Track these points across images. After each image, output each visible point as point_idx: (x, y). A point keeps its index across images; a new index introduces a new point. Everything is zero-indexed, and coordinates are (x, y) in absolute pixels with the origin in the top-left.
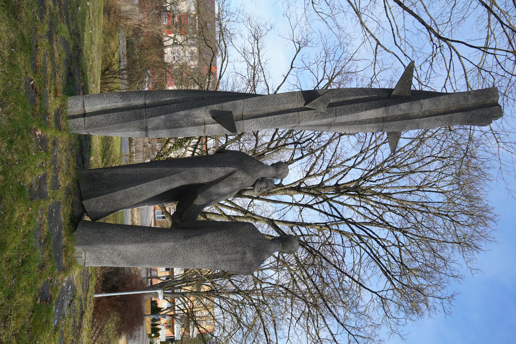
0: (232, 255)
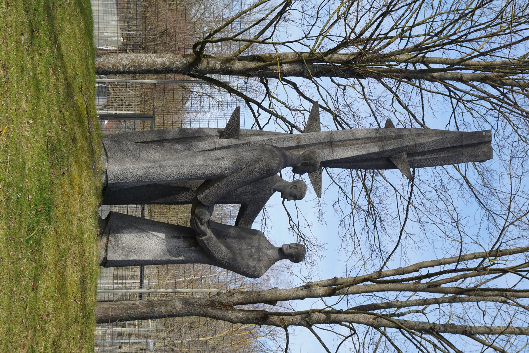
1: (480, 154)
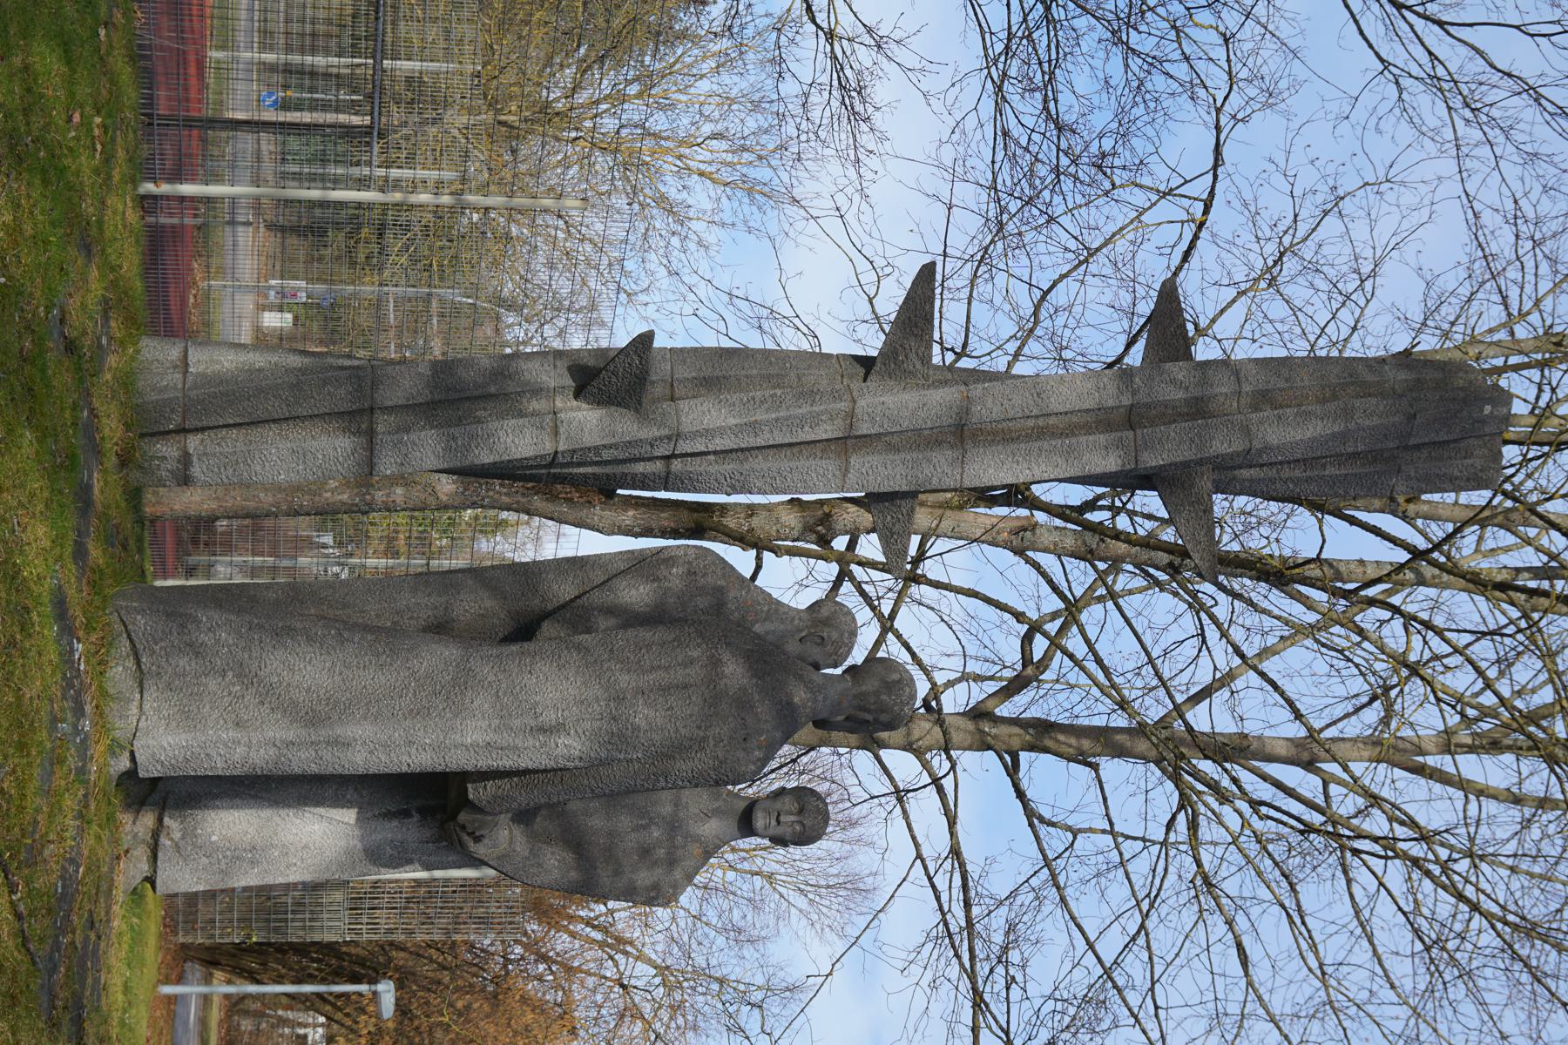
0: (672, 672)
1: (1456, 473)
